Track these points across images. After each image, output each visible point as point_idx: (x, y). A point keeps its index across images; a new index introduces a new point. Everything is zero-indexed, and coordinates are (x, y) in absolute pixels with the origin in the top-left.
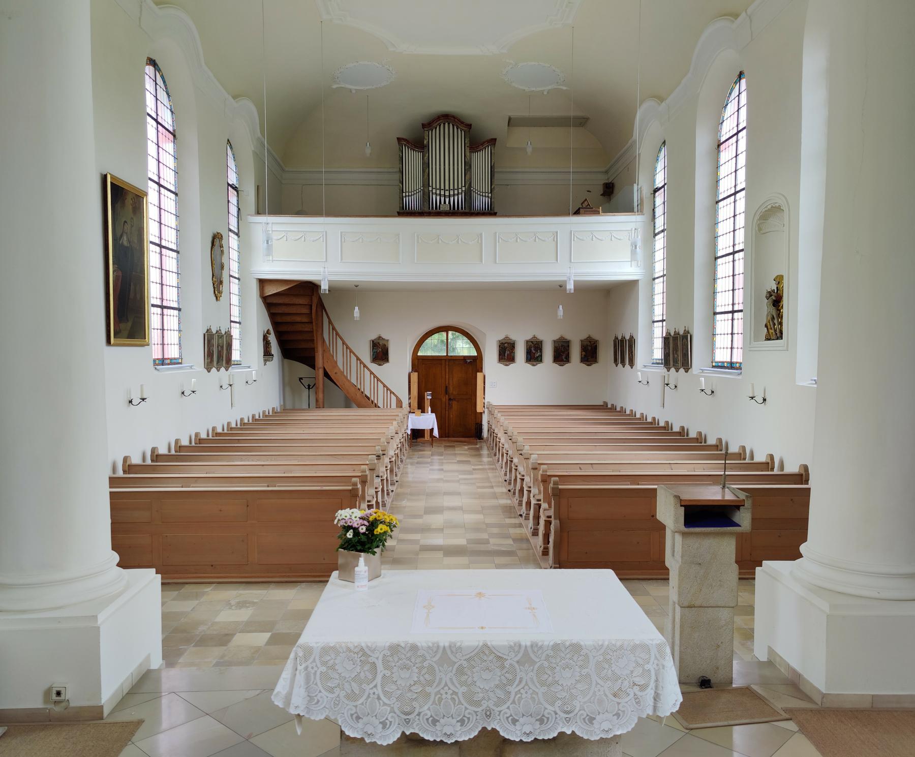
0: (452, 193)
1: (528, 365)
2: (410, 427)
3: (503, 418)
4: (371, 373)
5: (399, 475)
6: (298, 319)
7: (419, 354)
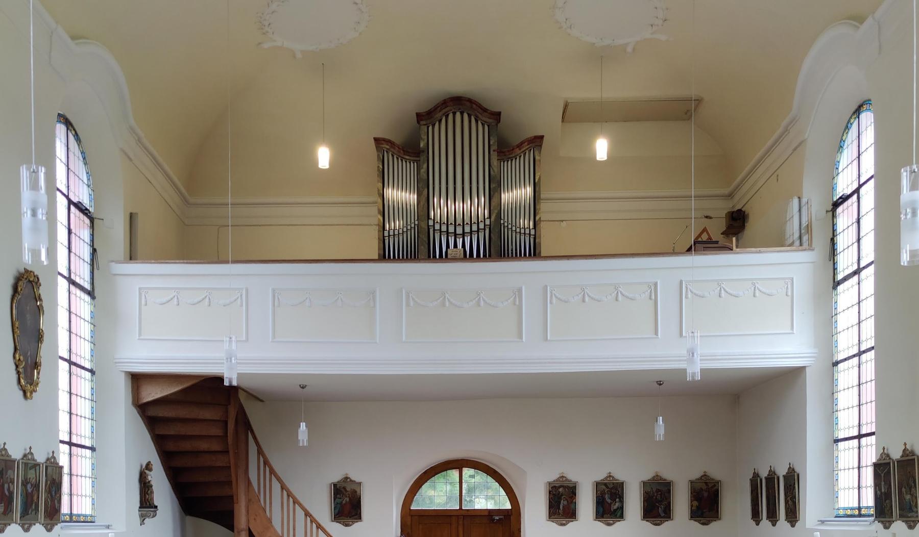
1: (599, 525)
6: (204, 446)
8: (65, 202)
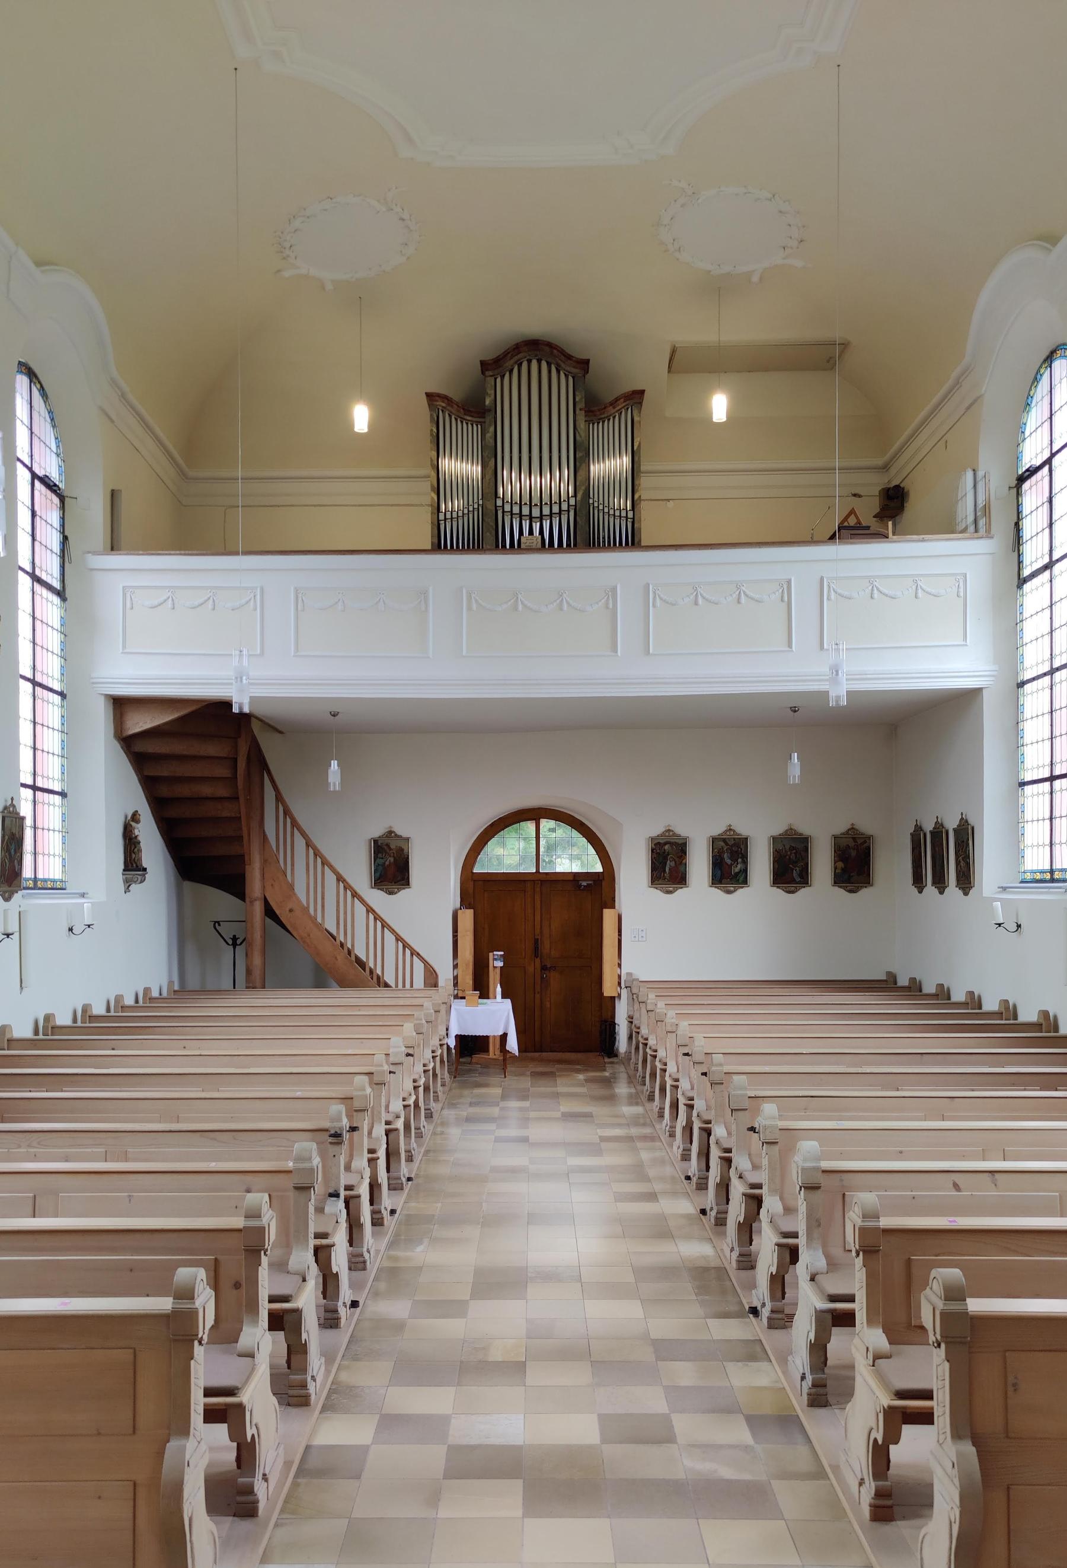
0: (546, 511)
2: (454, 1031)
3: (671, 1013)
4: (370, 910)
5: (418, 1158)
6: (206, 790)
7: (477, 870)
8: (27, 475)
